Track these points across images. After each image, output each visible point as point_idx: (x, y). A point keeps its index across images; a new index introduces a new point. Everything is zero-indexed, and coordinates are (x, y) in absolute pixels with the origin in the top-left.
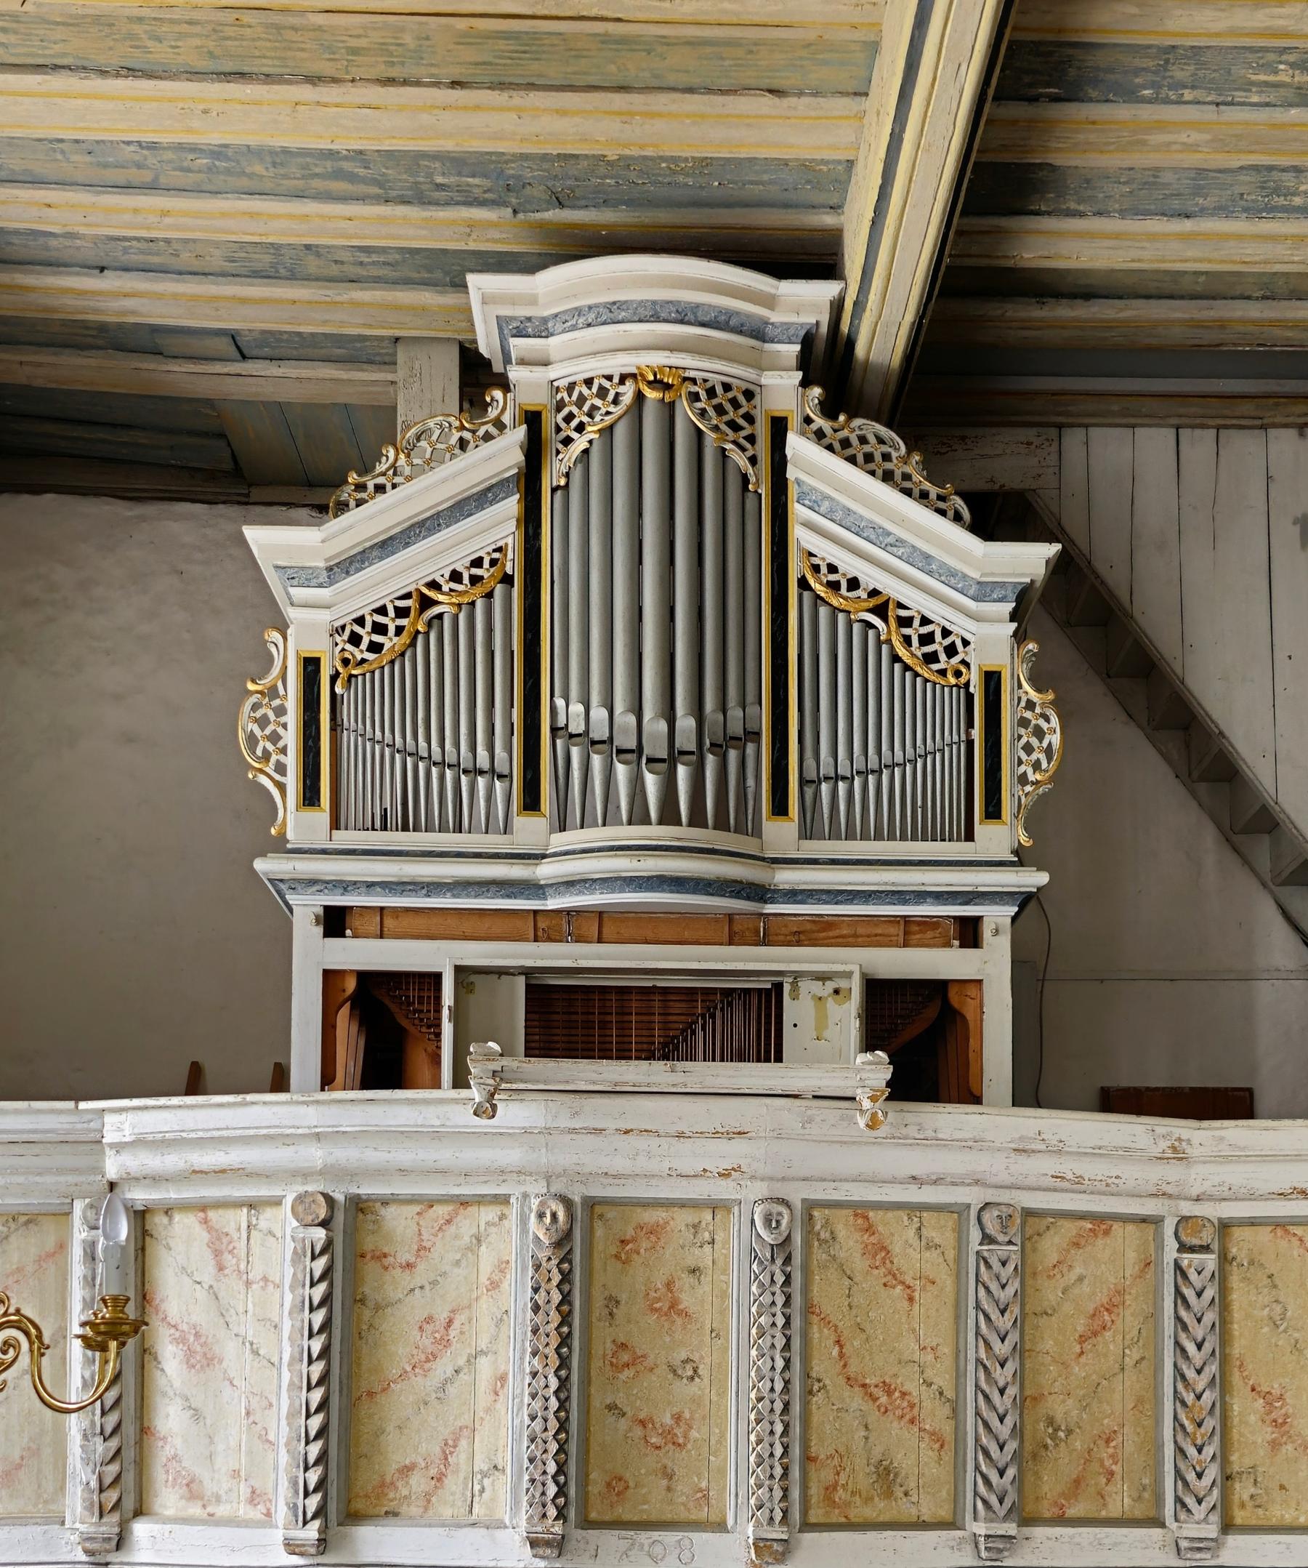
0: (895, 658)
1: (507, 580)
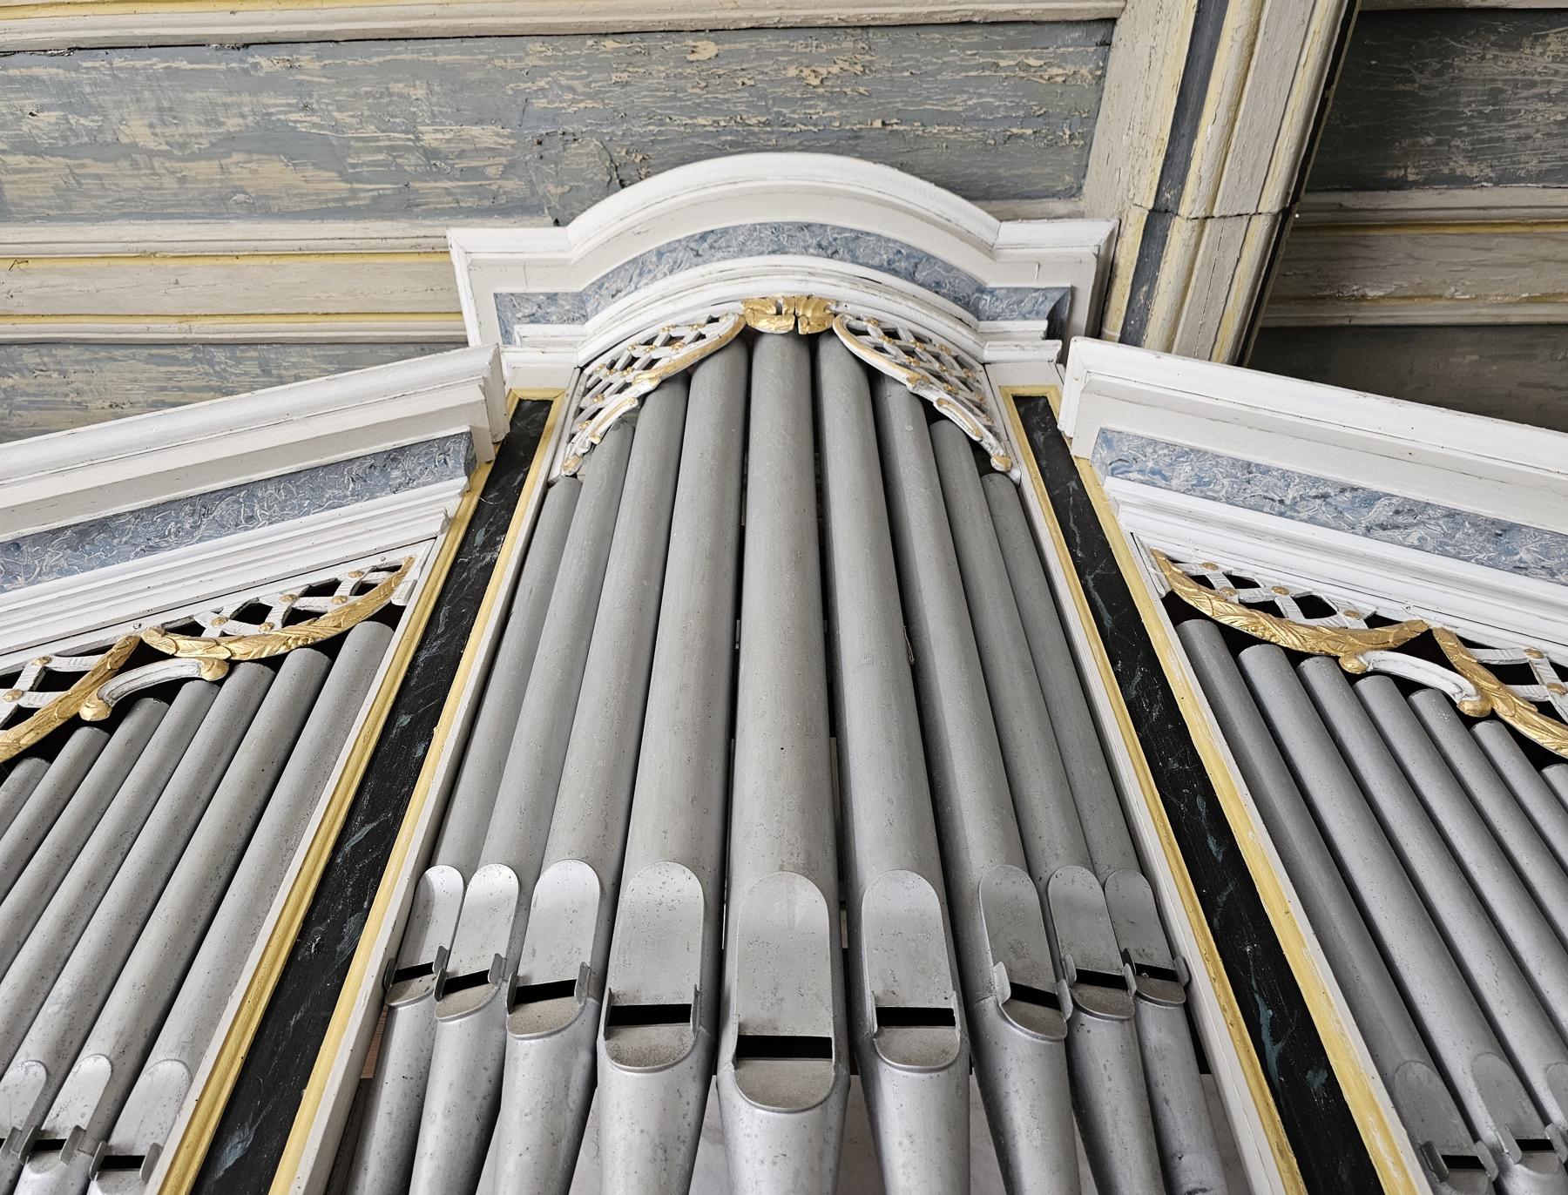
1: (390, 616)
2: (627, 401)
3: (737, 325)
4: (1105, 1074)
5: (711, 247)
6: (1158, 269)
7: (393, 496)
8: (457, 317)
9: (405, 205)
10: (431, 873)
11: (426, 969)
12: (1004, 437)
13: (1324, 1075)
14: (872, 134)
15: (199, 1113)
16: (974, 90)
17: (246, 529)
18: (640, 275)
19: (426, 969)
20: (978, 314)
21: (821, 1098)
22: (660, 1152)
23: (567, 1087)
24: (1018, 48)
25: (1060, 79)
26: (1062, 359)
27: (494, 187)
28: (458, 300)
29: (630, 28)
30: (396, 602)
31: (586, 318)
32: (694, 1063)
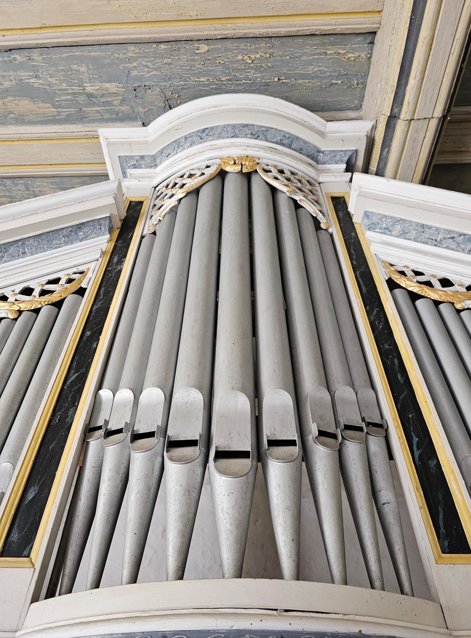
1: (81, 292)
2: (172, 202)
3: (217, 169)
4: (353, 462)
5: (207, 135)
6: (391, 141)
7: (80, 243)
8: (104, 165)
9: (80, 118)
10: (100, 392)
11: (100, 428)
12: (326, 214)
13: (435, 462)
14: (274, 83)
15: (18, 481)
16: (314, 64)
17: (22, 257)
18: (178, 147)
19: (100, 428)
20: (317, 162)
21: (246, 473)
22: (187, 492)
23: (153, 470)
24: (335, 45)
25: (352, 59)
26: (351, 181)
27: (117, 109)
28: (104, 158)
29: (171, 39)
30: (83, 286)
31: (156, 166)
32: (200, 461)
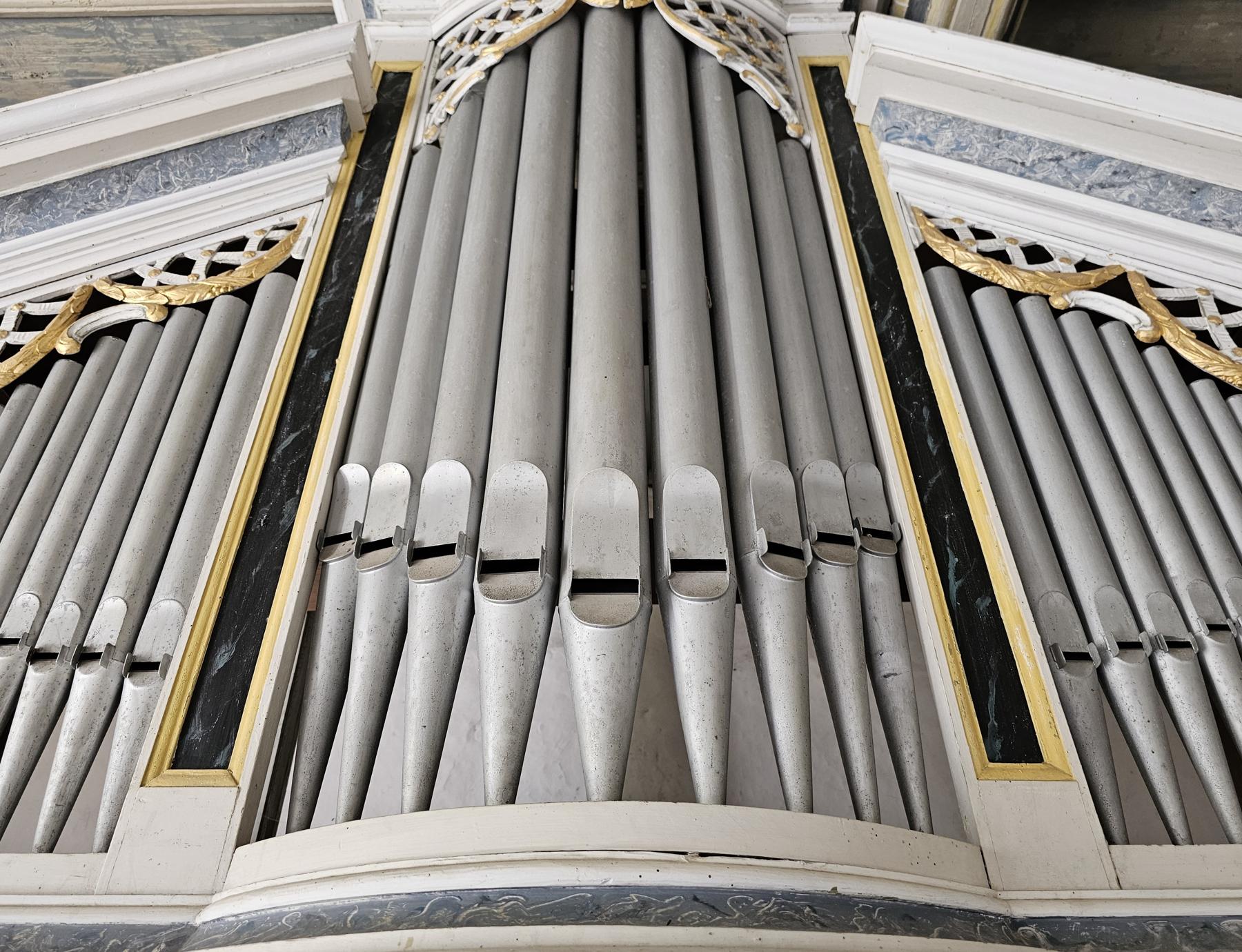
0: (1189, 373)
1: (291, 268)
